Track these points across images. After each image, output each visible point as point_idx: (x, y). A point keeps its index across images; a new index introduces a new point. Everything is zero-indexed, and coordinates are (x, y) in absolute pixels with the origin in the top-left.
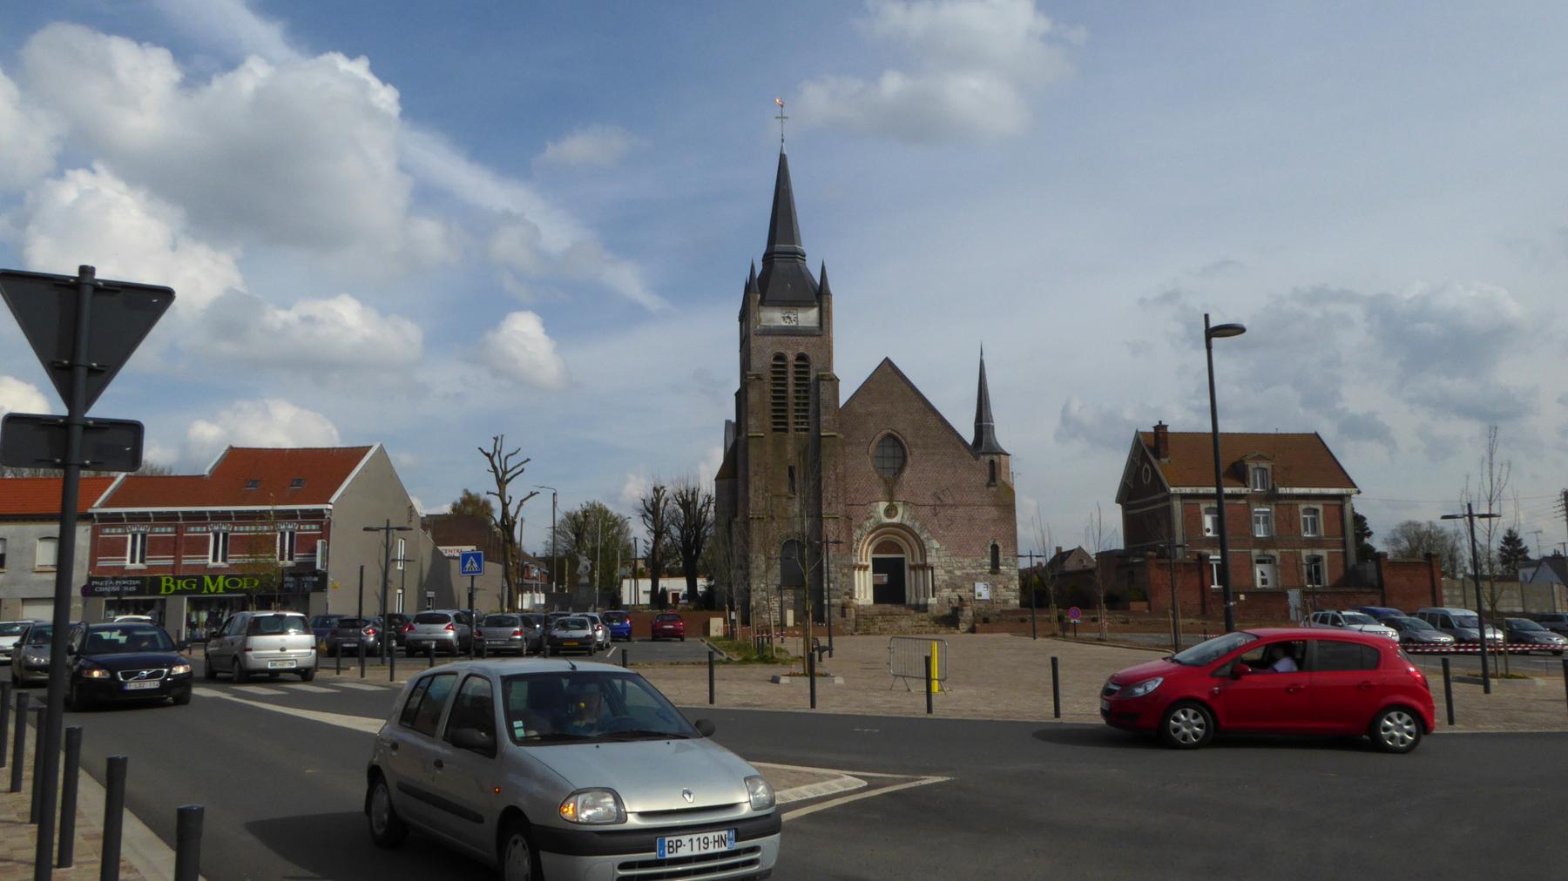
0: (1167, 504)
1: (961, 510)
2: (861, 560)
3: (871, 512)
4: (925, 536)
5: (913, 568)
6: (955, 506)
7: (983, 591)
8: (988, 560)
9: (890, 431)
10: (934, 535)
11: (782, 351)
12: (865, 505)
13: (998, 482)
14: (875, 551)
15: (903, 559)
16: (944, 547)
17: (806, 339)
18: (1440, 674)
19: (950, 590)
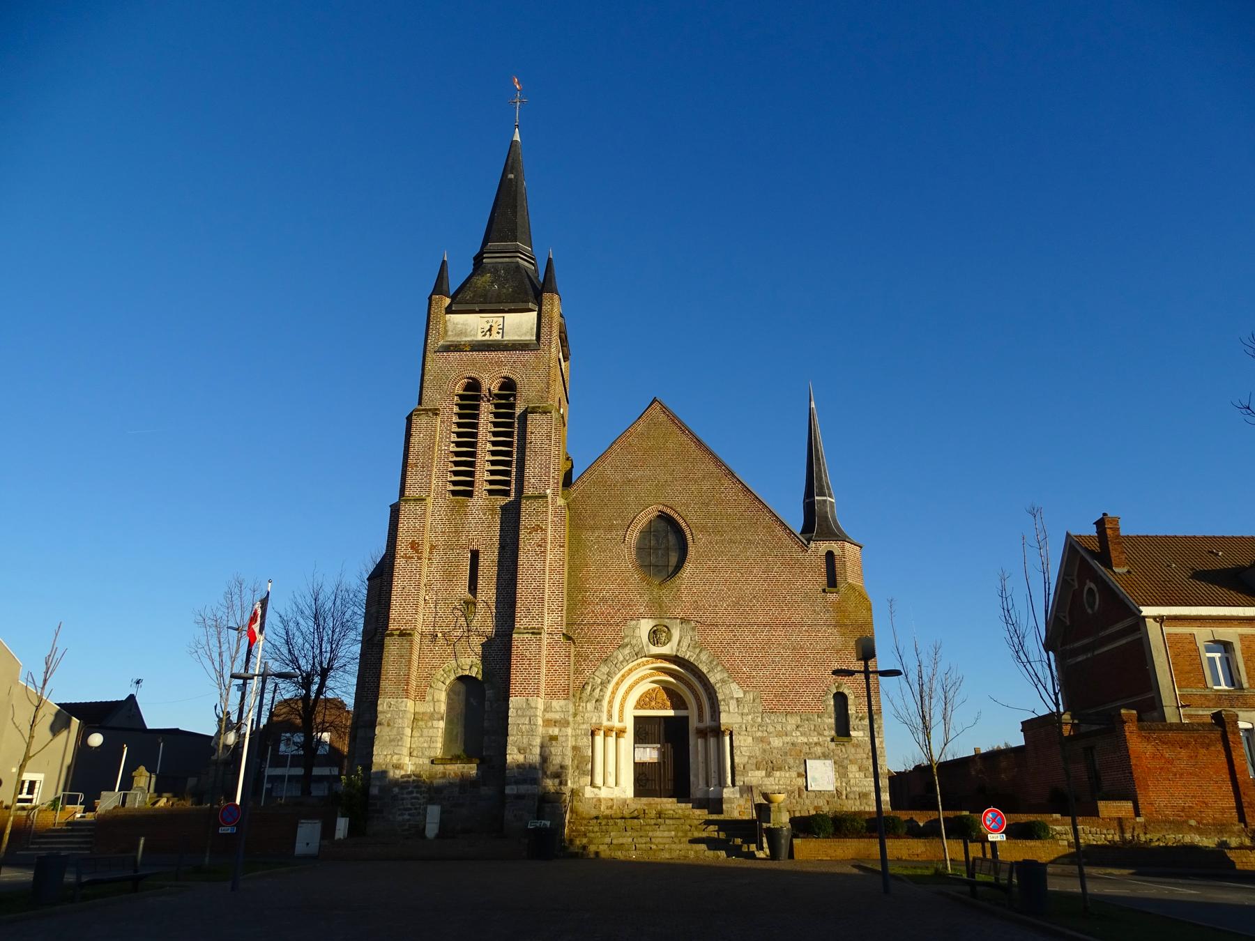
0: (1136, 636)
2: (610, 717)
4: (719, 676)
7: (822, 776)
9: (661, 507)
10: (733, 674)
13: (842, 587)
15: (687, 718)
16: (750, 696)
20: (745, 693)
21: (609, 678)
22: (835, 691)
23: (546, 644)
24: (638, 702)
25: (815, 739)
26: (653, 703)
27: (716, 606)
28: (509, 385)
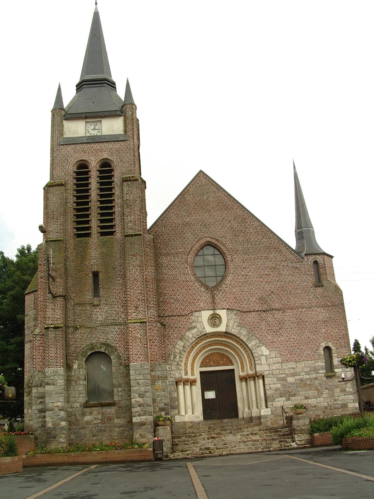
1: (289, 313)
2: (186, 373)
5: (243, 379)
8: (321, 363)
9: (208, 239)
14: (203, 365)
15: (233, 370)
17: (111, 145)
19: (284, 398)
21: (185, 349)
23: (148, 329)
24: (202, 363)
25: (314, 376)
26: (212, 363)
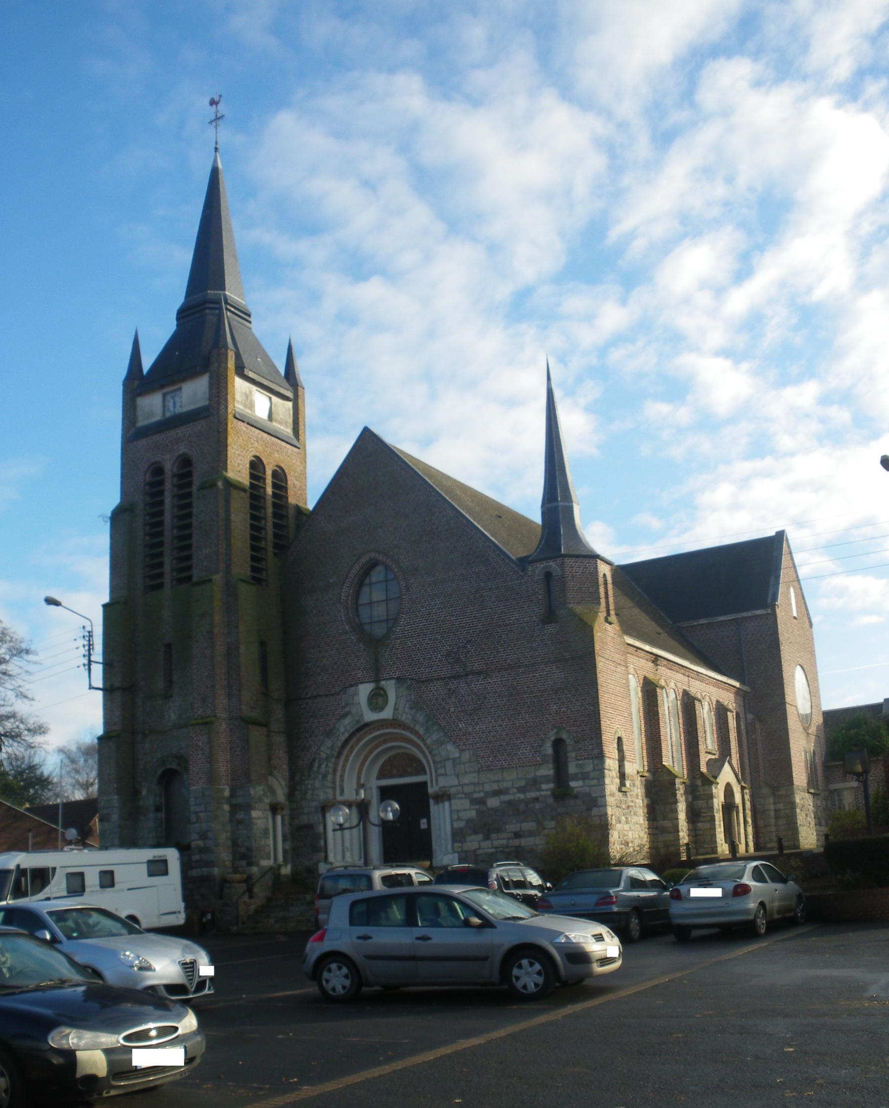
3: (347, 705)
4: (435, 737)
6: (484, 673)
11: (157, 459)
12: (338, 693)
14: (381, 775)
15: (424, 785)
16: (466, 756)
18: (798, 786)
19: (480, 837)
20: (462, 751)
22: (553, 738)
27: (430, 659)
28: (186, 462)
